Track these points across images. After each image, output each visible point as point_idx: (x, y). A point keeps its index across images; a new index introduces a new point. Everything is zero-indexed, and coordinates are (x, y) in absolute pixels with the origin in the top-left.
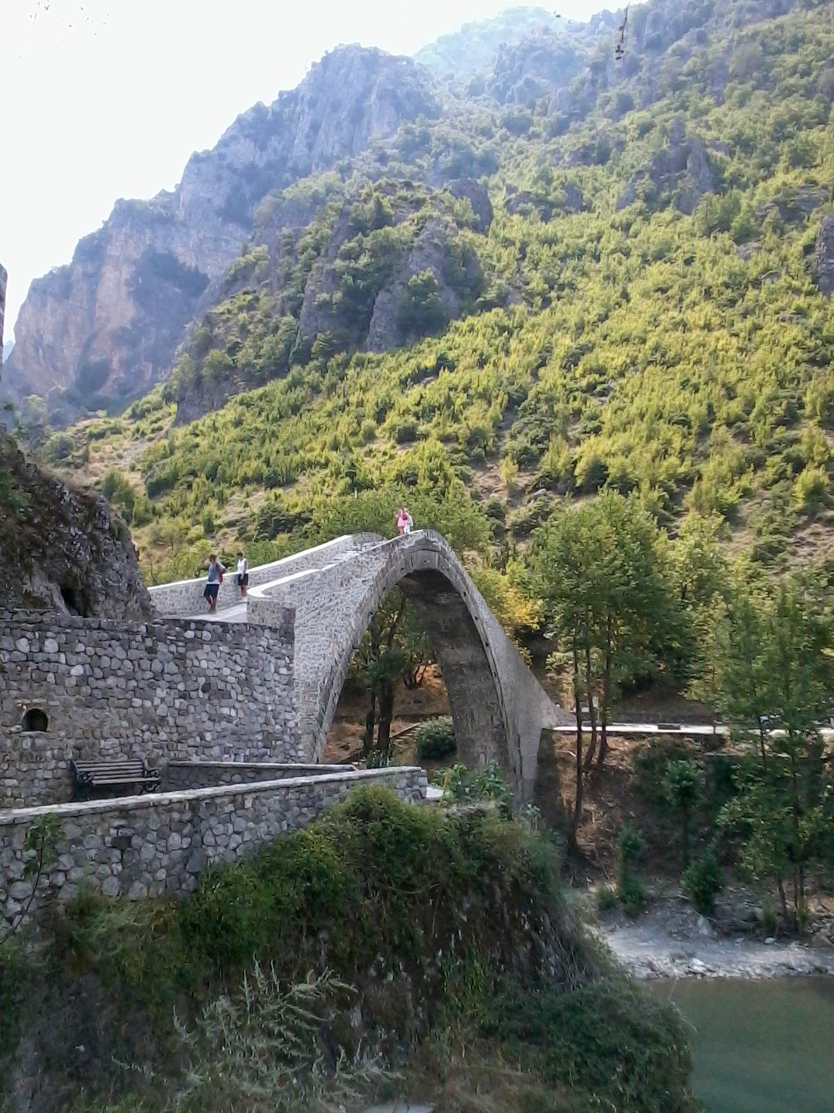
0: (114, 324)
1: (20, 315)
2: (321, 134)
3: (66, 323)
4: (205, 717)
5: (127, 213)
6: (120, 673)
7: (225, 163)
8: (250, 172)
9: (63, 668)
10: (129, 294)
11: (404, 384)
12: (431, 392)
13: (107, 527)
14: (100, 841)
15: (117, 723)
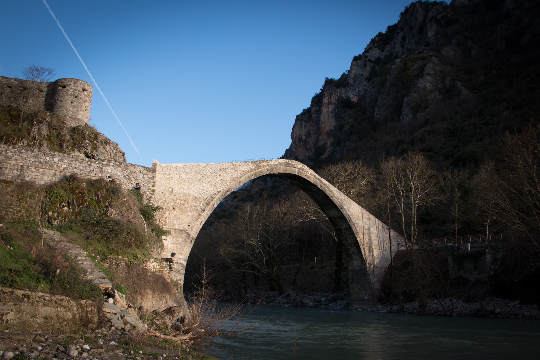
0: (327, 129)
1: (293, 130)
2: (407, 41)
7: (367, 59)
9: (59, 165)
10: (332, 116)
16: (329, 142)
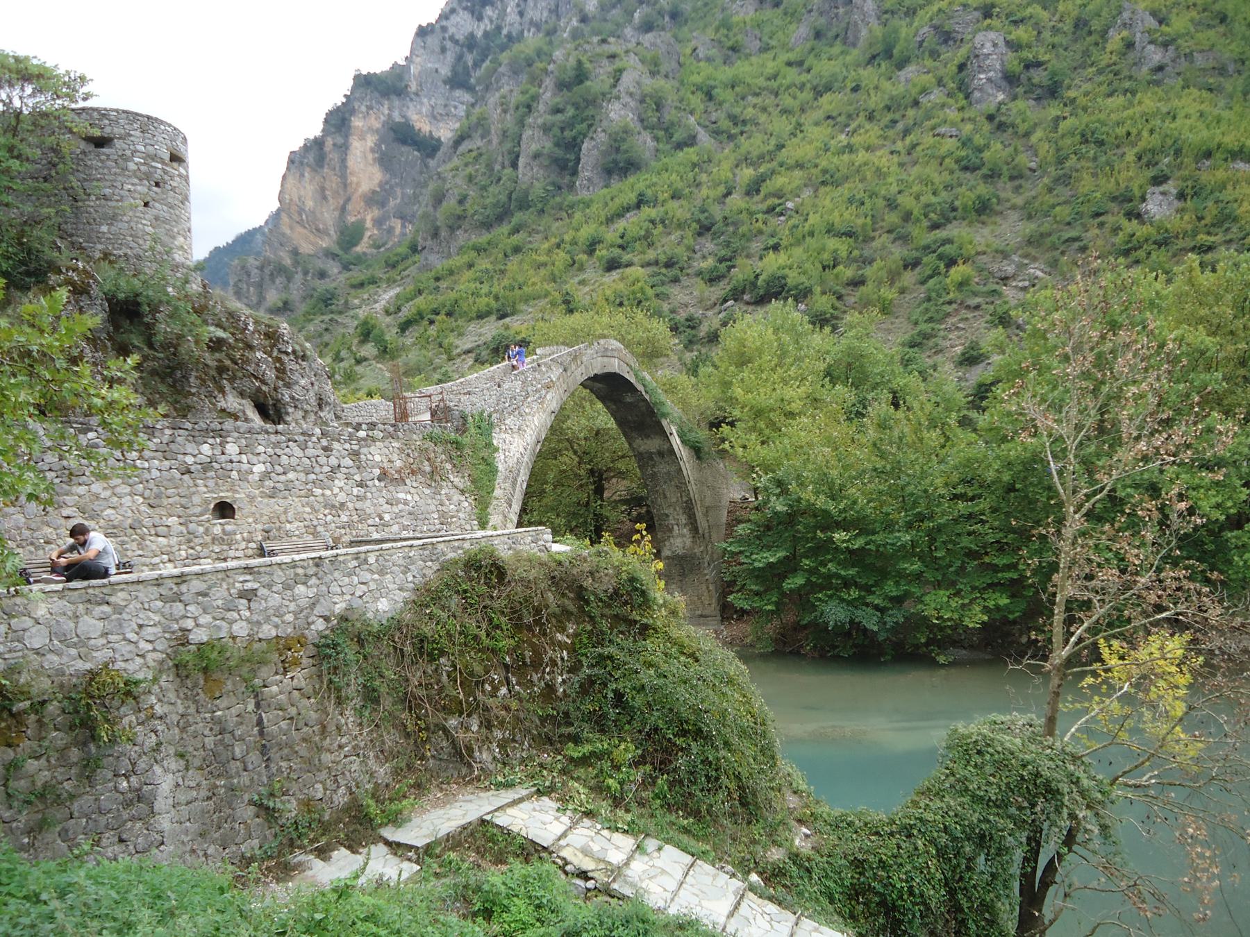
1: (282, 185)
3: (323, 189)
4: (382, 501)
5: (373, 87)
6: (299, 468)
8: (471, 42)
9: (245, 467)
10: (374, 159)
11: (609, 220)
12: (632, 224)
13: (290, 350)
14: (226, 593)
15: (300, 509)
16: (369, 218)
